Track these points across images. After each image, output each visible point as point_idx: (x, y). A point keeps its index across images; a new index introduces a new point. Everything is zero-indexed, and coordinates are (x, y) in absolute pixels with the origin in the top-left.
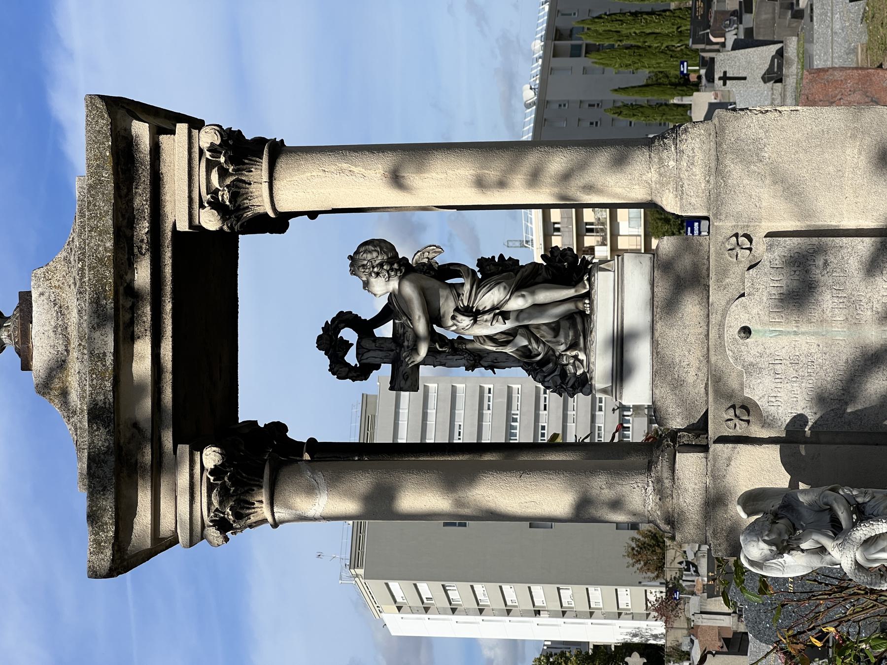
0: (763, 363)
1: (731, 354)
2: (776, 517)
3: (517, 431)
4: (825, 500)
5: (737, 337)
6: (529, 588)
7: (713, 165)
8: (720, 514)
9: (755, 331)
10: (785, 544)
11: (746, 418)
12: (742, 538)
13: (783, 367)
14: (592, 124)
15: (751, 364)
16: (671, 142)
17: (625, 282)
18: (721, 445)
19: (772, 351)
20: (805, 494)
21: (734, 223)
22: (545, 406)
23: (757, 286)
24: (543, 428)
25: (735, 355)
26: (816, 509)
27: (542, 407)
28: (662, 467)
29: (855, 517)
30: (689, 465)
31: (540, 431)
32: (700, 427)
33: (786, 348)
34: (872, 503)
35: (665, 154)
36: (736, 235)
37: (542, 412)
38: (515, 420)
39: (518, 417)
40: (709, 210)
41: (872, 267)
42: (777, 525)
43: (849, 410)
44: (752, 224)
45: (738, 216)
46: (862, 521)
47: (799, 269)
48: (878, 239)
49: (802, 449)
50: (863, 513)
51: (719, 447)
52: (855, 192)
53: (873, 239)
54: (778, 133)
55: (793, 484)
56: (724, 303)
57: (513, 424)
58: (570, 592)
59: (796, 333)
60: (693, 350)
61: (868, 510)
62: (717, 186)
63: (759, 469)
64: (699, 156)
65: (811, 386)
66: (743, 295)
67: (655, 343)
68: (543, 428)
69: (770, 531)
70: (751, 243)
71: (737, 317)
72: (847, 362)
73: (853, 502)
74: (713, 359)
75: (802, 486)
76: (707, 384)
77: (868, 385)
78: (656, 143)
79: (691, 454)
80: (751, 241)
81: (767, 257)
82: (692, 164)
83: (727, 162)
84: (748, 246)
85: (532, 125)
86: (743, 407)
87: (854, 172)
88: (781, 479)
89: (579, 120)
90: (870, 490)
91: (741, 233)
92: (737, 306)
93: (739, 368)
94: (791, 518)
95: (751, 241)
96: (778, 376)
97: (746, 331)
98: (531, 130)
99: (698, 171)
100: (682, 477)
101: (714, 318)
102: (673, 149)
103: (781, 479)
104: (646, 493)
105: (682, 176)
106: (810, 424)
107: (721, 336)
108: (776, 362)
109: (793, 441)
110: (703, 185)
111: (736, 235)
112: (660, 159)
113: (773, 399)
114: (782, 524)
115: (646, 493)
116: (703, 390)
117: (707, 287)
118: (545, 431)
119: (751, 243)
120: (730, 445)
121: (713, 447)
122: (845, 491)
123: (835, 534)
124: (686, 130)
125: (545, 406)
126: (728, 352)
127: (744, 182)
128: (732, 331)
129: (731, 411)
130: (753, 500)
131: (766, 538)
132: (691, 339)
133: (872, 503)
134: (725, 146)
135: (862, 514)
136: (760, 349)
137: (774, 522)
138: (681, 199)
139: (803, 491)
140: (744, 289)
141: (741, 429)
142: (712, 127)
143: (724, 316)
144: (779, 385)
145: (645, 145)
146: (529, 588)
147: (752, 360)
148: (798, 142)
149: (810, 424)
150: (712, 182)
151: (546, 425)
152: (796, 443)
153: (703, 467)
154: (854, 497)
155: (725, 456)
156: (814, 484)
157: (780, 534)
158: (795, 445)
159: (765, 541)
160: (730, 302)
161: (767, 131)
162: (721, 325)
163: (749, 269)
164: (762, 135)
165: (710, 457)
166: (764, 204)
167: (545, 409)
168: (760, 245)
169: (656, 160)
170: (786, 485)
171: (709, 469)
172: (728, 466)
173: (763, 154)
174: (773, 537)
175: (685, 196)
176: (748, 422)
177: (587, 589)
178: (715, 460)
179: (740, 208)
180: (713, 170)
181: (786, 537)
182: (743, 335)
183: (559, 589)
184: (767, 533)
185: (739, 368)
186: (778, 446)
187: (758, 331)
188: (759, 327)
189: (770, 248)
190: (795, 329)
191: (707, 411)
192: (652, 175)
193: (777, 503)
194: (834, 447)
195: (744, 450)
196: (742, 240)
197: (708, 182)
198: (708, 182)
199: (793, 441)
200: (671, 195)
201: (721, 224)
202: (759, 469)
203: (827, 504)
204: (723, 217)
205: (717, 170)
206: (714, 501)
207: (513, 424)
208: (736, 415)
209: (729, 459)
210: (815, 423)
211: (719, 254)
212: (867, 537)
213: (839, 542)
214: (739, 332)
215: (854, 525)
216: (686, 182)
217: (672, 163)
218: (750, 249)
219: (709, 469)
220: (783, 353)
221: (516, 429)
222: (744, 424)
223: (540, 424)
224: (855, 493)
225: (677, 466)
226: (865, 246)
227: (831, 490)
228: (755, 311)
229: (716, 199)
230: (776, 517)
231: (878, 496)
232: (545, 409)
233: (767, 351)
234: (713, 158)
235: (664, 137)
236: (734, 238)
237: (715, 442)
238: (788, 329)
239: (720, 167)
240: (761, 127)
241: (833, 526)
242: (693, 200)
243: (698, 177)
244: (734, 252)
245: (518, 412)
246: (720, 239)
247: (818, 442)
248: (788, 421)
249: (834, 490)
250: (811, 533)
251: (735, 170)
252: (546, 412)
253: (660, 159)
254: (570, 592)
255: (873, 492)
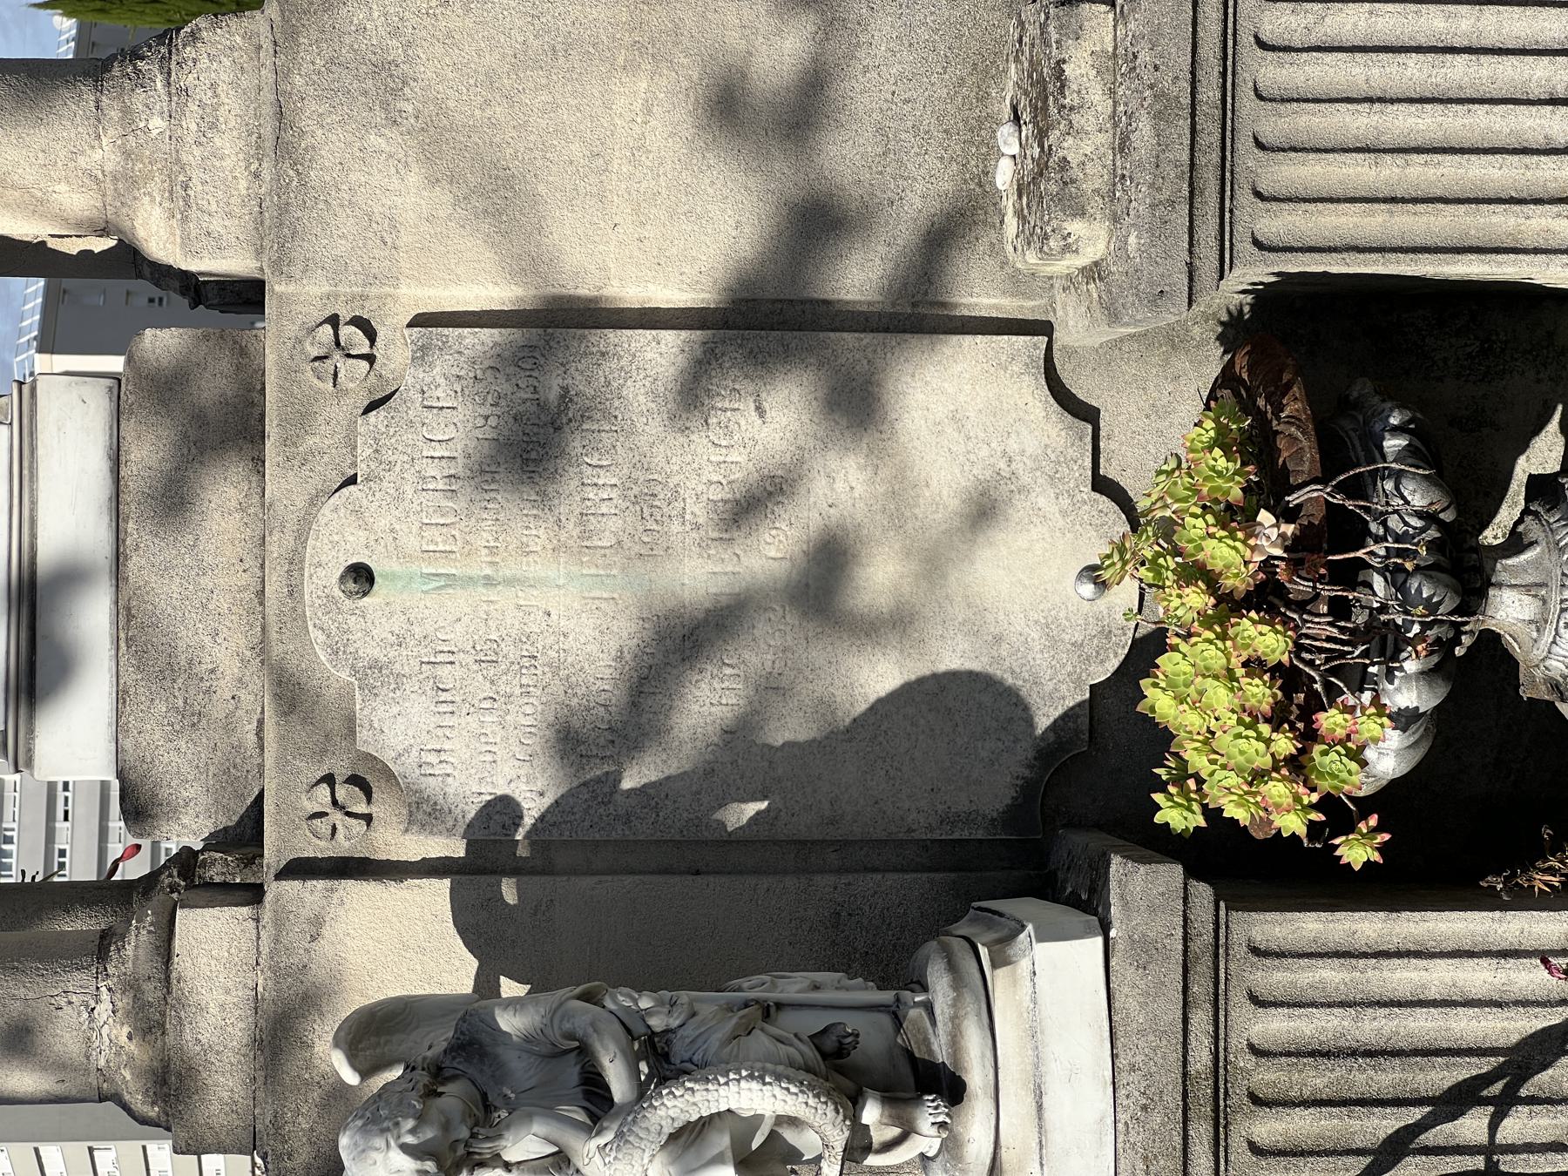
0: (406, 660)
1: (322, 638)
2: (438, 1073)
3: (13, 860)
4: (567, 1026)
5: (337, 593)
6: (36, 1150)
7: (268, 131)
8: (293, 1067)
9: (385, 577)
10: (461, 1151)
11: (361, 808)
12: (344, 1141)
13: (458, 672)
14: (151, 300)
15: (375, 665)
16: (155, 68)
17: (40, 452)
18: (297, 884)
19: (429, 629)
20: (516, 1014)
21: (326, 289)
22: (66, 813)
23: (388, 455)
24: (62, 853)
25: (337, 640)
26: (545, 1050)
27: (60, 815)
28: (136, 945)
29: (644, 1067)
30: (211, 942)
31: (57, 859)
32: (243, 836)
33: (465, 620)
34: (689, 1032)
35: (138, 99)
36: (334, 321)
37: (60, 825)
38: (9, 840)
39: (14, 834)
40: (259, 253)
41: (692, 395)
42: (440, 1102)
43: (627, 784)
44: (373, 291)
45: (339, 269)
46: (663, 1081)
47: (497, 411)
48: (697, 335)
49: (509, 891)
50: (666, 1057)
51: (292, 887)
52: (636, 211)
53: (684, 334)
54: (439, 49)
55: (486, 985)
56: (301, 501)
57: (5, 847)
58: (112, 1155)
59: (489, 582)
60: (224, 632)
61: (679, 1051)
62: (280, 187)
63: (402, 945)
64: (231, 106)
65: (529, 721)
66: (352, 480)
67: (125, 615)
68: (62, 853)
69: (421, 1118)
70: (372, 340)
71: (340, 537)
72: (620, 657)
73: (639, 1029)
74: (277, 650)
75: (510, 988)
76: (261, 722)
77: (675, 718)
78: (116, 71)
79: (216, 911)
80: (371, 335)
81: (412, 378)
82: (213, 126)
83: (306, 123)
84: (365, 350)
85: (40, 300)
86: (355, 780)
87: (633, 160)
88: (451, 970)
89: (128, 293)
90: (684, 996)
91: (345, 315)
92: (336, 510)
93: (344, 675)
94: (479, 1079)
95: (371, 335)
96: (443, 696)
97: (361, 576)
98: (38, 310)
99: (230, 147)
100: (189, 974)
101: (277, 546)
102: (159, 85)
103: (451, 970)
104: (91, 1020)
105: (184, 157)
106: (528, 821)
107: (294, 591)
108: (440, 658)
109: (489, 863)
110: (243, 184)
111: (334, 321)
112: (126, 111)
113: (433, 758)
114: (453, 1096)
115: (91, 1020)
116: (252, 738)
117: (259, 461)
118: (66, 860)
119: (372, 340)
120: (320, 884)
121: (273, 889)
122: (621, 999)
123: (595, 1118)
124: (194, 37)
125: (66, 813)
126: (315, 634)
127: (353, 177)
128: (323, 576)
129: (324, 790)
130: (374, 1032)
131: (409, 1139)
132: (222, 602)
133: (689, 1032)
134: (298, 80)
135: (664, 1062)
136: (398, 624)
137: (431, 1093)
138: (185, 219)
139: (514, 1004)
140: (354, 464)
141: (348, 841)
142: (264, 28)
143: (302, 536)
144: (449, 720)
145: (86, 74)
146: (36, 1150)
147: (376, 653)
148: (491, 78)
149: (528, 821)
150: (266, 175)
151: (67, 847)
152: (493, 872)
153: (247, 944)
154: (642, 1015)
155: (306, 913)
156: (540, 984)
157: (446, 1127)
158: (492, 879)
159: (405, 1148)
160: (314, 501)
161: (409, 44)
162: (295, 561)
163: (367, 410)
164: (397, 53)
165: (267, 915)
166: (405, 239)
167: (66, 819)
168: (396, 347)
169: (115, 114)
170: (465, 985)
171: (265, 950)
172: (313, 939)
173: (401, 105)
174: (429, 1133)
175: (193, 213)
176: (368, 818)
177: (144, 1148)
178: (279, 924)
179: (342, 248)
180: (269, 144)
181: (464, 1133)
182: (351, 586)
183: (91, 1150)
184: (410, 1123)
185: (344, 675)
186: (447, 882)
187: (392, 577)
188: (396, 567)
189: (422, 354)
190: (488, 571)
191: (261, 795)
192: (104, 155)
193: (437, 1040)
194: (587, 882)
195: (353, 890)
196: (347, 332)
197: (257, 175)
198: (257, 175)
199: (489, 863)
200: (157, 211)
201: (291, 288)
202: (402, 945)
203: (570, 1036)
204: (296, 271)
205: (280, 140)
206: (276, 1033)
207: (5, 847)
208: (335, 802)
209: (317, 922)
210: (542, 818)
211: (289, 372)
212: (678, 1124)
213: (608, 1136)
214: (342, 579)
215: (642, 1093)
216: (197, 176)
217: (157, 123)
218: (370, 359)
219: (265, 950)
220: (457, 636)
221: (9, 855)
222: (358, 826)
223: (57, 847)
224: (645, 1003)
225: (177, 943)
226: (662, 352)
227: (580, 997)
228: (383, 523)
229: (277, 222)
230: (438, 1073)
231: (706, 1010)
232: (66, 819)
233: (417, 629)
234: (268, 110)
235: (136, 55)
236: (328, 329)
237: (282, 875)
238: (469, 572)
239: (287, 136)
240: (395, 33)
241: (588, 1096)
242: (216, 225)
243: (228, 163)
244: (328, 365)
245: (15, 826)
246: (292, 329)
247: (547, 870)
248: (471, 815)
249: (587, 997)
250: (529, 1117)
251: (329, 139)
252: (68, 824)
253: (126, 111)
254: (112, 1155)
255: (691, 1004)
